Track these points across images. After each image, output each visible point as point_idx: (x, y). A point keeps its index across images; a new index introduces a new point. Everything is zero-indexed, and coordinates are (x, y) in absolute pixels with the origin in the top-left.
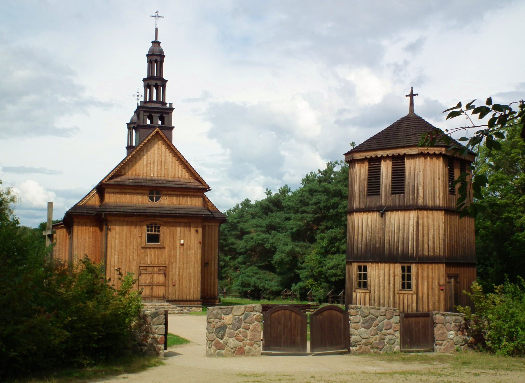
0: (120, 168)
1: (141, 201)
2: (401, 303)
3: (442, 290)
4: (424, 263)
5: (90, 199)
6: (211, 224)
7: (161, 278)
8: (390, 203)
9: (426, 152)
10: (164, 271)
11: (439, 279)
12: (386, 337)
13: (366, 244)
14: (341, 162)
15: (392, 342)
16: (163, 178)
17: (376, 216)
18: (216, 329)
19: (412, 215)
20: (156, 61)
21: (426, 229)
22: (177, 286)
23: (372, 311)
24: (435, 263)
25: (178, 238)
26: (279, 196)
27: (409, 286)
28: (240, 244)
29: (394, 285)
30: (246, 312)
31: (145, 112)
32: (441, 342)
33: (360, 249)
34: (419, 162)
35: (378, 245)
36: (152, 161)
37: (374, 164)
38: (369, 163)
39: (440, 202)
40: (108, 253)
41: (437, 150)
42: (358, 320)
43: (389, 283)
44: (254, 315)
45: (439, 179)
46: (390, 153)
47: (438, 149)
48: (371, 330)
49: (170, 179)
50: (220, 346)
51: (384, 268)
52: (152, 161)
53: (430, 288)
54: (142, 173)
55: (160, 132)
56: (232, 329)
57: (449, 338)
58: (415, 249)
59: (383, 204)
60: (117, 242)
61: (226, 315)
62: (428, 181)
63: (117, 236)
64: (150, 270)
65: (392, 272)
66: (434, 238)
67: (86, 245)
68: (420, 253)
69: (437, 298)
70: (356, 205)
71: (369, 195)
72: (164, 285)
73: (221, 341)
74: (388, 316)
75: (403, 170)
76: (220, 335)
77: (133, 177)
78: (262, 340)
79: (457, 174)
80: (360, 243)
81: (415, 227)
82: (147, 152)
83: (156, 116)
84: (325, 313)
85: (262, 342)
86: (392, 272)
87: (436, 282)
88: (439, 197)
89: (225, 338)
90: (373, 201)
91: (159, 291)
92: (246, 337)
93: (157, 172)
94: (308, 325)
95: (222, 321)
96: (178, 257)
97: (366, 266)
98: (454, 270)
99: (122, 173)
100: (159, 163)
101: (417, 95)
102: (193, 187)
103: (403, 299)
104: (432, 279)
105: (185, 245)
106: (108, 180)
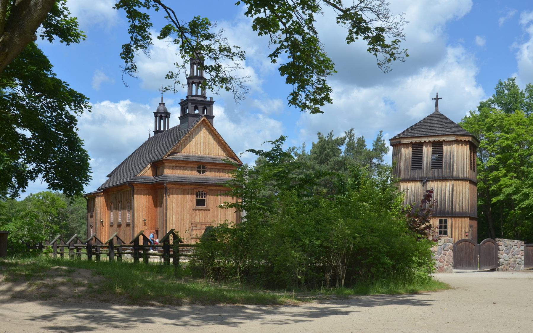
1: (192, 174)
5: (146, 172)
9: (460, 139)
14: (300, 148)
16: (207, 156)
17: (419, 184)
21: (458, 193)
34: (455, 147)
36: (199, 143)
37: (417, 147)
40: (168, 213)
41: (467, 139)
46: (431, 139)
52: (199, 143)
55: (206, 120)
59: (425, 176)
62: (460, 159)
70: (402, 176)
75: (441, 152)
77: (185, 154)
82: (195, 136)
87: (463, 230)
93: (203, 151)
99: (177, 151)
100: (205, 144)
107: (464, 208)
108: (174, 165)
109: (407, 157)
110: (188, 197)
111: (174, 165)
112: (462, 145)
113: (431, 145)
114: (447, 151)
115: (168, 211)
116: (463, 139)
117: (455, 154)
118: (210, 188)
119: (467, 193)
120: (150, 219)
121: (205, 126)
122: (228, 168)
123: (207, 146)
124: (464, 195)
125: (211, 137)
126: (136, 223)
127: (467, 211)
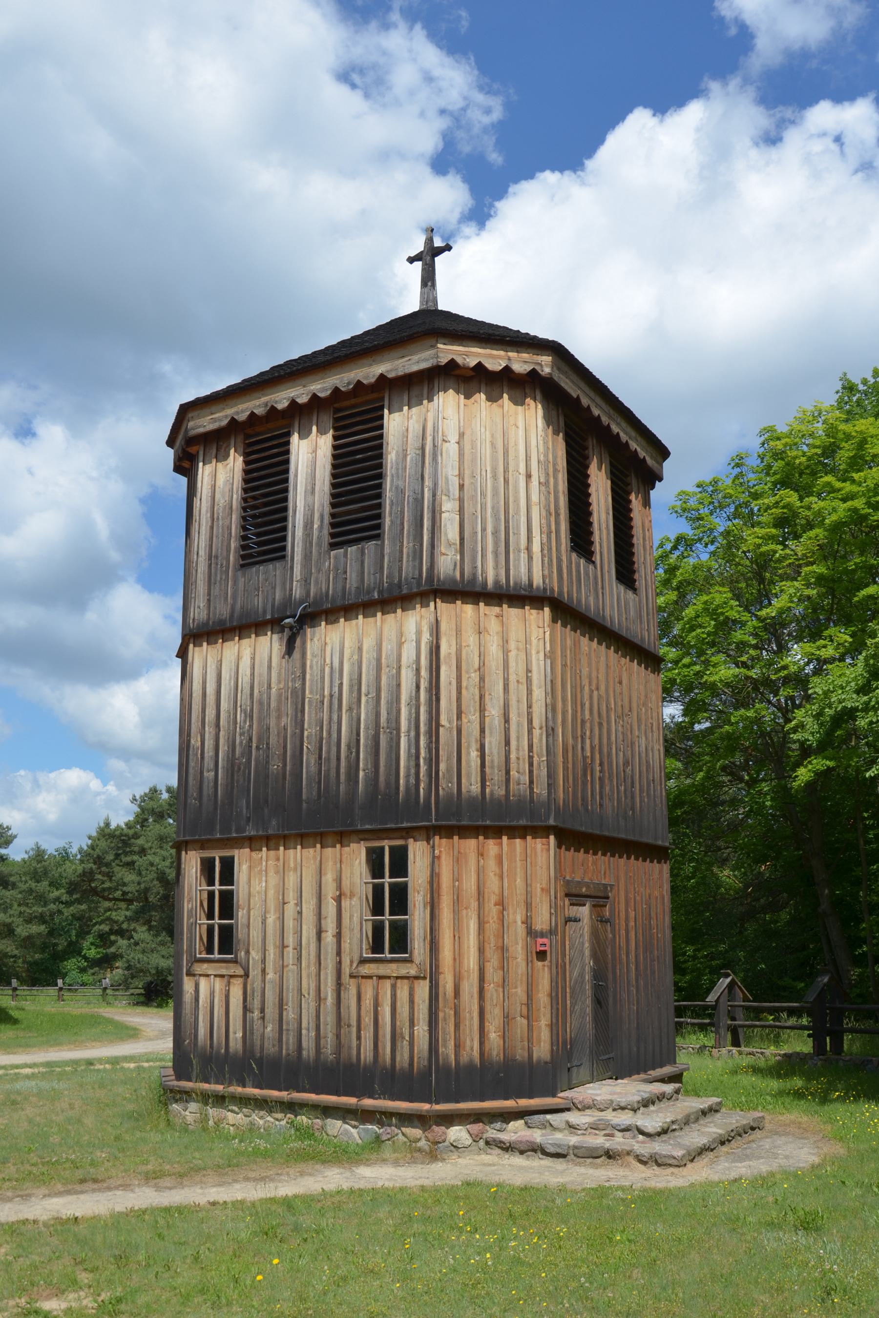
2: (368, 1020)
3: (541, 955)
4: (465, 831)
8: (324, 584)
11: (528, 906)
17: (268, 645)
19: (413, 622)
21: (471, 679)
29: (339, 936)
34: (447, 406)
35: (275, 766)
37: (264, 449)
38: (246, 455)
39: (532, 567)
43: (320, 933)
45: (529, 476)
47: (525, 356)
51: (302, 860)
53: (493, 947)
58: (423, 768)
59: (297, 592)
65: (329, 878)
68: (447, 785)
69: (520, 992)
71: (242, 566)
75: (375, 449)
81: (424, 673)
86: (329, 878)
87: (517, 916)
88: (529, 549)
97: (233, 858)
98: (594, 868)
103: (376, 1005)
104: (501, 903)
107: (519, 775)
113: (328, 420)
119: (537, 677)
124: (517, 693)
126: (390, 965)
127: (541, 790)
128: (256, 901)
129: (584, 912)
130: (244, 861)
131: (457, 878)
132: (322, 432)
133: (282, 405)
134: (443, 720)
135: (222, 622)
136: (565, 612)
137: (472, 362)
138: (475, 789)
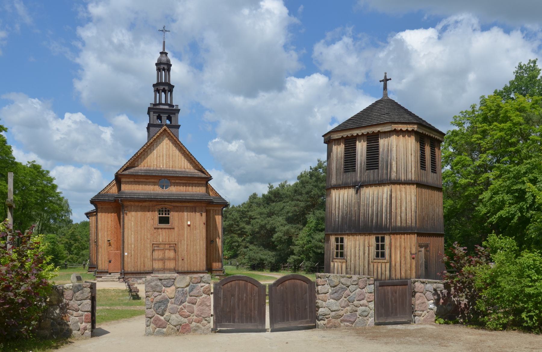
0: (134, 161)
2: (375, 271)
3: (413, 258)
5: (111, 189)
6: (215, 208)
7: (172, 254)
8: (365, 178)
10: (174, 247)
11: (411, 248)
12: (358, 309)
13: (343, 217)
15: (365, 314)
16: (171, 169)
17: (352, 191)
18: (156, 303)
19: (386, 189)
20: (164, 69)
21: (399, 202)
22: (185, 260)
23: (343, 280)
24: (407, 234)
25: (186, 220)
26: (278, 190)
27: (383, 255)
28: (248, 228)
29: (369, 254)
30: (191, 284)
31: (154, 113)
32: (421, 312)
33: (337, 223)
34: (394, 139)
35: (353, 218)
36: (161, 155)
37: (350, 143)
38: (345, 144)
39: (412, 176)
41: (410, 128)
42: (325, 291)
43: (364, 254)
44: (202, 287)
45: (411, 154)
46: (365, 131)
48: (342, 301)
49: (177, 169)
50: (160, 323)
54: (152, 165)
55: (167, 129)
56: (175, 304)
57: (430, 307)
58: (388, 221)
59: (358, 180)
60: (133, 224)
61: (167, 287)
62: (402, 156)
63: (133, 219)
64: (162, 247)
65: (366, 242)
66: (406, 210)
67: (109, 227)
68: (393, 224)
69: (409, 265)
70: (334, 181)
72: (175, 259)
73: (162, 318)
74: (361, 285)
75: (377, 147)
76: (160, 310)
77: (145, 168)
78: (212, 315)
79: (428, 149)
80: (337, 216)
82: (157, 147)
83: (164, 117)
84: (287, 282)
85: (212, 318)
86: (366, 242)
87: (408, 251)
89: (167, 314)
90: (350, 178)
91: (171, 265)
92: (193, 313)
93: (166, 164)
94: (267, 297)
95: (163, 294)
96: (186, 236)
99: (136, 165)
101: (390, 79)
102: (197, 176)
103: (377, 268)
104: (405, 248)
105: (191, 226)
106: (123, 171)
107: (409, 222)
108: (132, 180)
109: (339, 156)
110: (149, 214)
111: (132, 180)
112: (404, 136)
113: (365, 138)
114: (384, 145)
115: (126, 230)
116: (404, 127)
117: (394, 149)
118: (175, 204)
119: (413, 200)
120: (115, 239)
121: (167, 137)
122: (196, 182)
123: (171, 159)
125: (175, 148)
128: (349, 247)
129: (423, 249)
130: (346, 239)
131: (395, 243)
132: (364, 141)
133: (355, 135)
134: (393, 211)
135: (340, 185)
136: (419, 185)
137: (399, 129)
138: (399, 225)
